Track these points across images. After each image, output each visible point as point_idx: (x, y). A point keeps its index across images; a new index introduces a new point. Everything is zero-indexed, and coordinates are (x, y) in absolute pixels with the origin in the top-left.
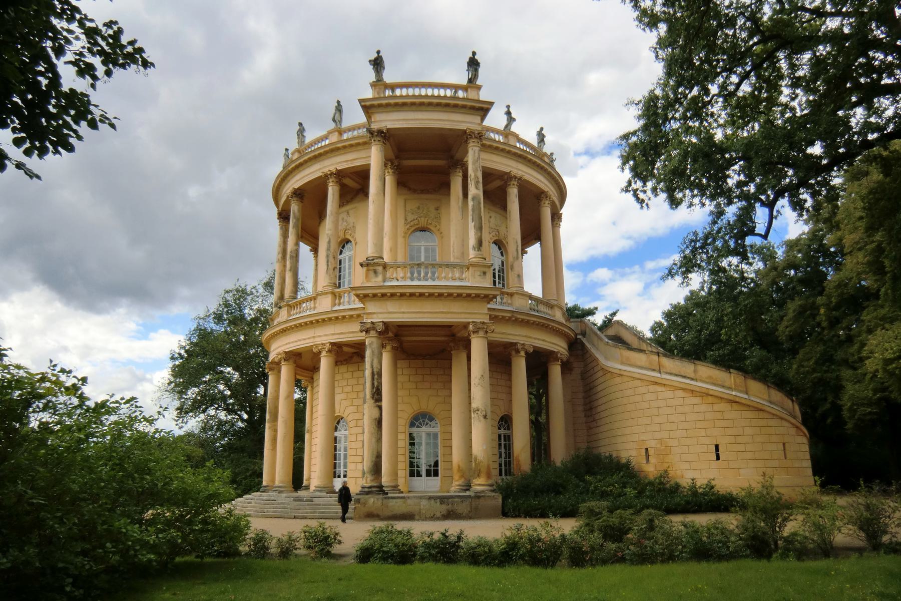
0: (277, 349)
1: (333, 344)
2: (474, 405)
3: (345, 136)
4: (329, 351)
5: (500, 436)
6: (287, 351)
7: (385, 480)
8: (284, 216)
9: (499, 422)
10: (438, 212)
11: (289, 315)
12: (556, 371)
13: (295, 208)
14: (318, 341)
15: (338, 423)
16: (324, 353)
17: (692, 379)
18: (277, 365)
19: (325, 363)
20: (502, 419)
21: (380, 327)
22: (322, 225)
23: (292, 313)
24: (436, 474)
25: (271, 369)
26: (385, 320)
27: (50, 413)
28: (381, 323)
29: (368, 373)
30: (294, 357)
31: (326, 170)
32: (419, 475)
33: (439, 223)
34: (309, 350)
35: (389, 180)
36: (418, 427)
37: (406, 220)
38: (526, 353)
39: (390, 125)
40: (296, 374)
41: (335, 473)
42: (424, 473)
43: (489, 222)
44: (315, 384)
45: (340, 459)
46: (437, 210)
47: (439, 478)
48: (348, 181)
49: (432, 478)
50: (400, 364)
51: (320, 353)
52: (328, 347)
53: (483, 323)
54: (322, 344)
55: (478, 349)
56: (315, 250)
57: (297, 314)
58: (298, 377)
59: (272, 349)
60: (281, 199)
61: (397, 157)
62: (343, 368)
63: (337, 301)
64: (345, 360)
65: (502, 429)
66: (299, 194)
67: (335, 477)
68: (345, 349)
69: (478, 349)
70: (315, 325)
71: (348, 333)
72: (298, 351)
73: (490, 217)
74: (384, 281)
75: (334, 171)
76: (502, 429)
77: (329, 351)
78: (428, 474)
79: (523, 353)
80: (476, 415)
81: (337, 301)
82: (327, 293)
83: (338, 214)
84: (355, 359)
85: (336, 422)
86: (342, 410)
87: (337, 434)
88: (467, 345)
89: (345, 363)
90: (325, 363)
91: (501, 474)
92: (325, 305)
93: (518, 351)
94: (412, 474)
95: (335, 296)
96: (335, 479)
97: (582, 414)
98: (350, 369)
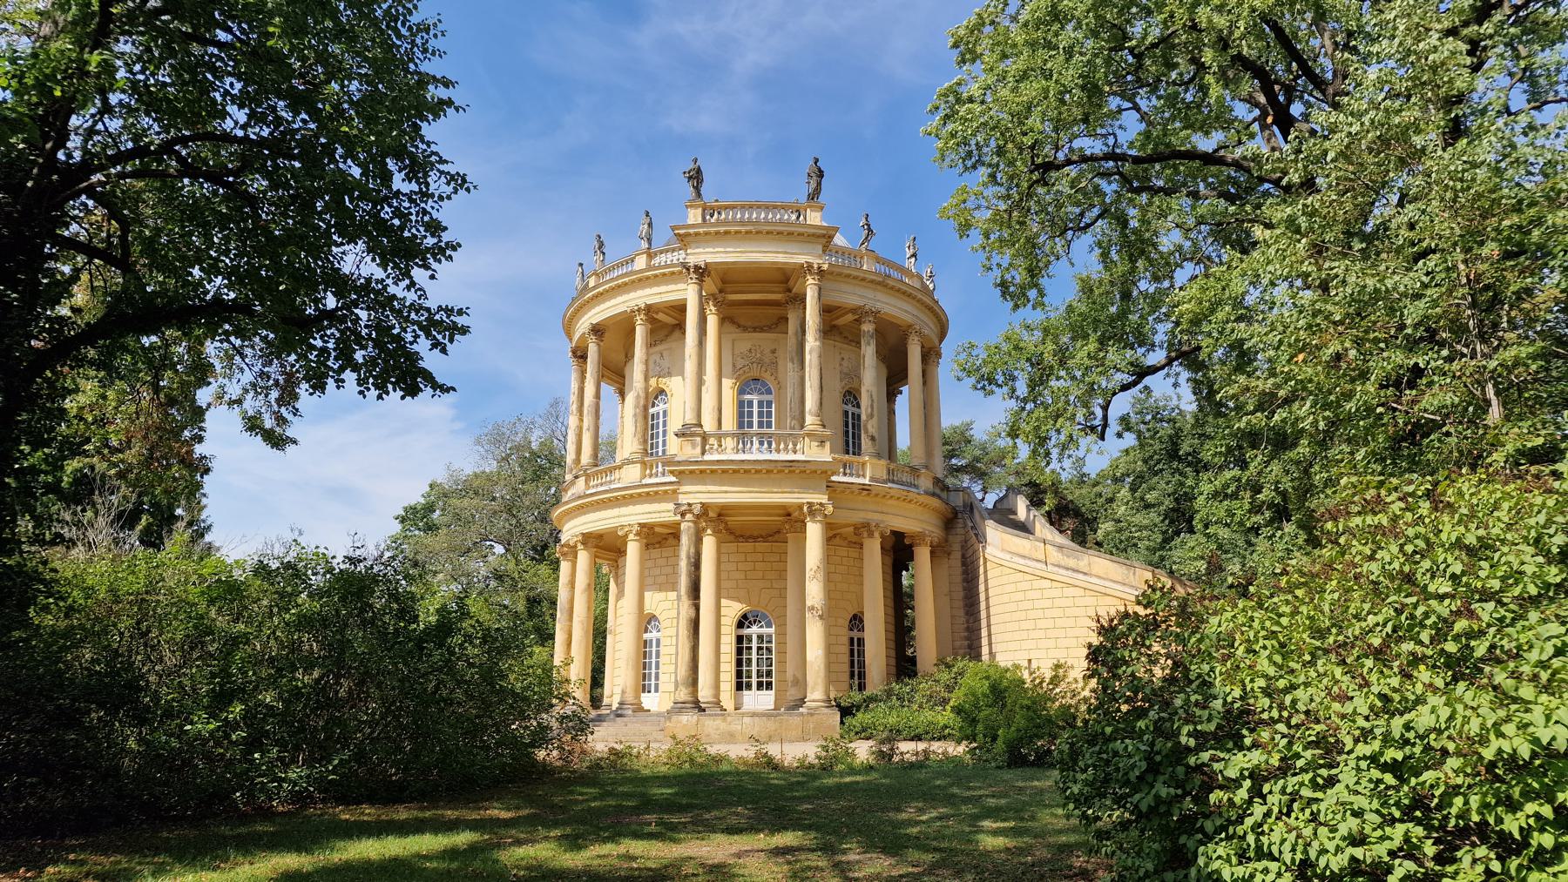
0: (571, 531)
1: (642, 525)
2: (809, 603)
3: (656, 261)
4: (637, 534)
5: (852, 640)
7: (704, 694)
8: (580, 355)
11: (587, 486)
12: (923, 555)
14: (624, 521)
15: (649, 623)
16: (631, 536)
17: (1085, 574)
18: (572, 552)
19: (633, 549)
21: (697, 509)
22: (628, 365)
24: (769, 686)
25: (564, 554)
27: (1158, 753)
29: (683, 565)
32: (749, 687)
34: (613, 532)
35: (712, 321)
37: (734, 366)
39: (710, 259)
41: (644, 686)
44: (620, 572)
45: (750, 677)
49: (765, 692)
52: (636, 528)
53: (821, 504)
55: (814, 532)
56: (622, 394)
61: (721, 291)
62: (655, 553)
66: (597, 330)
68: (657, 529)
70: (639, 637)
71: (661, 513)
74: (703, 453)
75: (643, 306)
77: (637, 534)
78: (760, 686)
79: (877, 535)
82: (633, 463)
83: (648, 354)
84: (671, 541)
85: (647, 621)
87: (646, 636)
90: (633, 549)
92: (631, 475)
93: (871, 535)
94: (739, 687)
98: (664, 554)
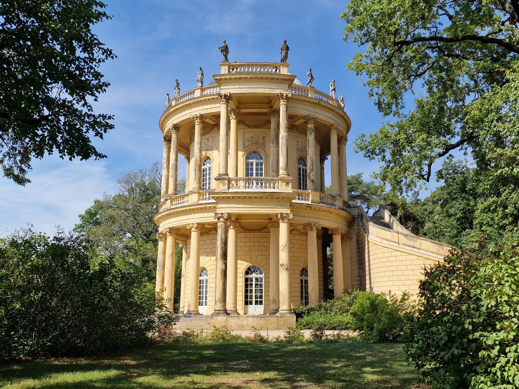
0: (164, 226)
1: (199, 224)
2: (281, 262)
3: (205, 93)
4: (196, 228)
6: (170, 227)
7: (229, 306)
9: (301, 272)
10: (264, 140)
12: (337, 239)
13: (174, 137)
14: (190, 222)
15: (202, 271)
16: (193, 229)
18: (164, 237)
19: (194, 236)
20: (303, 269)
21: (226, 216)
22: (192, 145)
23: (174, 203)
24: (261, 303)
25: (160, 238)
26: (229, 212)
28: (227, 214)
29: (219, 243)
30: (173, 231)
31: (193, 114)
33: (265, 147)
34: (184, 227)
35: (233, 123)
36: (251, 274)
37: (244, 145)
38: (317, 230)
40: (176, 239)
42: (254, 302)
43: (297, 145)
44: (188, 247)
46: (264, 139)
47: (263, 306)
48: (207, 120)
49: (259, 306)
50: (240, 235)
51: (191, 229)
52: (195, 225)
54: (192, 224)
56: (188, 159)
57: (176, 204)
58: (177, 241)
59: (160, 226)
60: (165, 128)
61: (237, 108)
62: (205, 237)
63: (201, 197)
64: (207, 232)
65: (304, 276)
66: (176, 127)
67: (200, 305)
69: (283, 228)
71: (208, 218)
72: (178, 227)
73: (298, 142)
74: (229, 188)
76: (304, 276)
77: (196, 228)
78: (256, 303)
79: (314, 229)
80: (281, 268)
81: (201, 197)
82: (194, 193)
83: (201, 139)
85: (201, 271)
86: (204, 264)
88: (277, 226)
89: (206, 234)
90: (194, 236)
91: (206, 280)
92: (193, 199)
93: (312, 229)
94: (246, 303)
95: (200, 194)
96: (199, 307)
97: (356, 268)
